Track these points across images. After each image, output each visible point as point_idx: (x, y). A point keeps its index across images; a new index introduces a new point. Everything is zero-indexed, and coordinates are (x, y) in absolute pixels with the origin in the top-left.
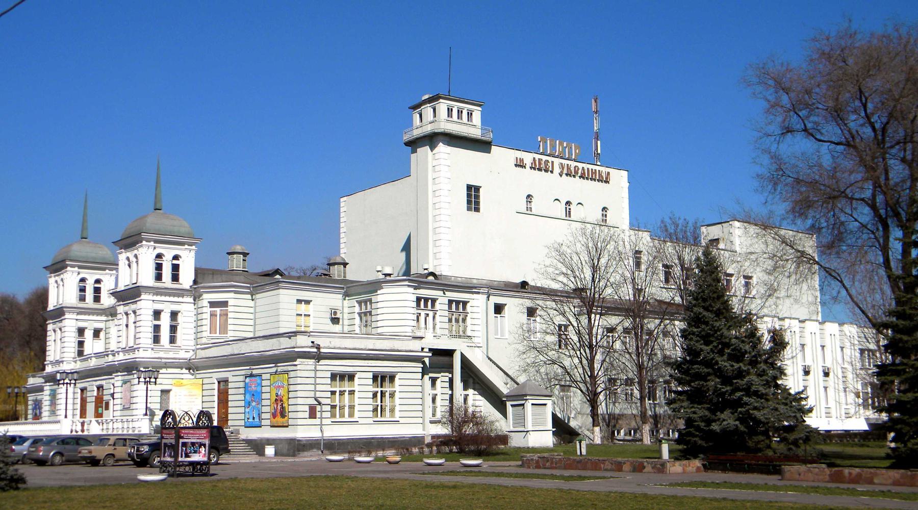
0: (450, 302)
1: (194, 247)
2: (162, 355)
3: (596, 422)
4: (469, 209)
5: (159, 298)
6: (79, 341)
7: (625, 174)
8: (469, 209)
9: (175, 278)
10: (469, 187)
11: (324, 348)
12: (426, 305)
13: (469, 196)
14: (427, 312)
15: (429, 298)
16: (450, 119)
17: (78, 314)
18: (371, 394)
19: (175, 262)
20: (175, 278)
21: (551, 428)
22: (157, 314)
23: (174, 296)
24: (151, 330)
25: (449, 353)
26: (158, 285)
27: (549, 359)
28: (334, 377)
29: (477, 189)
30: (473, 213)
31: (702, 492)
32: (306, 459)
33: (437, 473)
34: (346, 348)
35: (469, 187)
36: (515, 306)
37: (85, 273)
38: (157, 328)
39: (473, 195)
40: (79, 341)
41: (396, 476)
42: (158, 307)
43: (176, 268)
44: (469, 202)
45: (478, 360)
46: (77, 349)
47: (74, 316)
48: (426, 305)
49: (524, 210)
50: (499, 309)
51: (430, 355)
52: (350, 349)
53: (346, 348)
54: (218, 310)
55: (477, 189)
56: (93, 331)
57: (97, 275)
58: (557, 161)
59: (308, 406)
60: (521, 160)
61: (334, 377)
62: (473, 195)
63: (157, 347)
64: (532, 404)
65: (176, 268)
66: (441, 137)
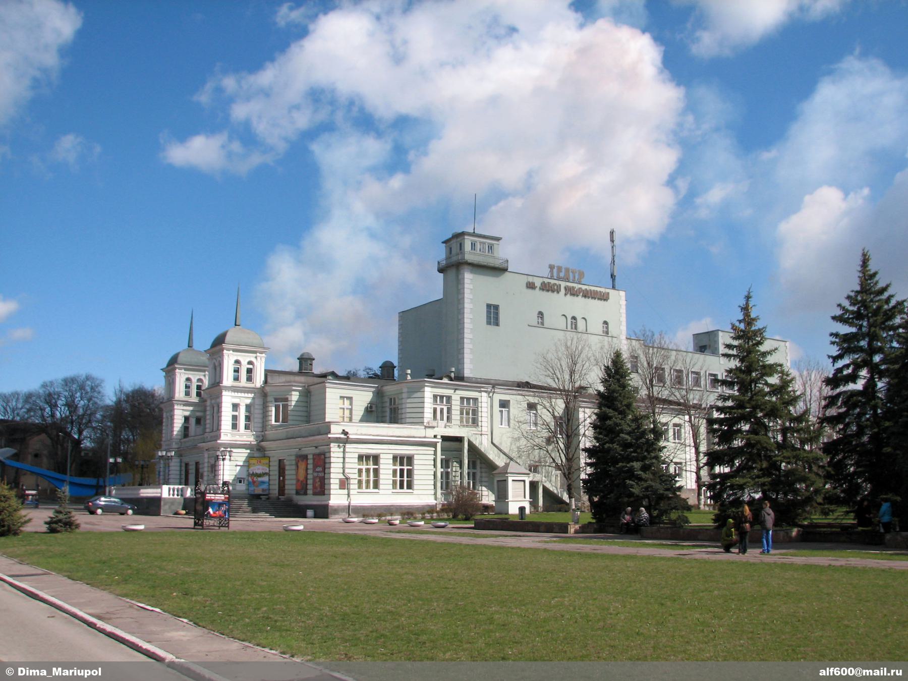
0: (462, 399)
1: (264, 355)
2: (237, 438)
3: (571, 495)
4: (489, 323)
5: (236, 394)
6: (233, 416)
7: (624, 292)
8: (489, 323)
9: (249, 379)
10: (489, 306)
11: (352, 434)
12: (442, 401)
13: (489, 312)
14: (442, 407)
15: (438, 395)
16: (473, 251)
17: (184, 405)
18: (357, 470)
19: (251, 366)
20: (249, 379)
21: (529, 499)
22: (235, 407)
23: (241, 392)
24: (230, 419)
25: (459, 440)
26: (236, 384)
27: (535, 443)
28: (361, 458)
29: (496, 307)
30: (493, 328)
31: (432, 538)
32: (334, 520)
33: (441, 533)
34: (370, 435)
35: (489, 306)
36: (518, 402)
37: (191, 375)
38: (235, 418)
39: (493, 314)
40: (233, 416)
41: (373, 532)
42: (236, 401)
43: (249, 371)
44: (489, 317)
45: (484, 445)
46: (231, 422)
47: (182, 407)
48: (442, 401)
49: (536, 324)
50: (504, 404)
51: (441, 440)
52: (373, 436)
53: (370, 435)
54: (281, 404)
55: (496, 307)
56: (245, 407)
57: (251, 357)
58: (563, 284)
59: (338, 480)
60: (533, 284)
61: (361, 458)
62: (493, 314)
63: (235, 432)
64: (513, 480)
65: (249, 371)
66: (466, 267)
